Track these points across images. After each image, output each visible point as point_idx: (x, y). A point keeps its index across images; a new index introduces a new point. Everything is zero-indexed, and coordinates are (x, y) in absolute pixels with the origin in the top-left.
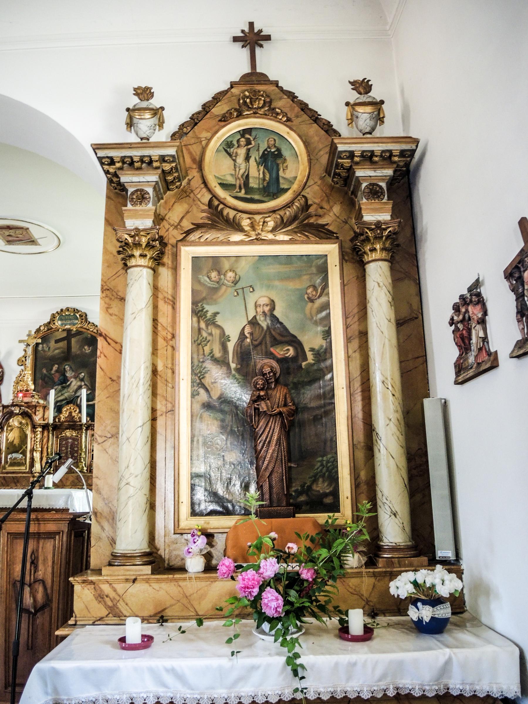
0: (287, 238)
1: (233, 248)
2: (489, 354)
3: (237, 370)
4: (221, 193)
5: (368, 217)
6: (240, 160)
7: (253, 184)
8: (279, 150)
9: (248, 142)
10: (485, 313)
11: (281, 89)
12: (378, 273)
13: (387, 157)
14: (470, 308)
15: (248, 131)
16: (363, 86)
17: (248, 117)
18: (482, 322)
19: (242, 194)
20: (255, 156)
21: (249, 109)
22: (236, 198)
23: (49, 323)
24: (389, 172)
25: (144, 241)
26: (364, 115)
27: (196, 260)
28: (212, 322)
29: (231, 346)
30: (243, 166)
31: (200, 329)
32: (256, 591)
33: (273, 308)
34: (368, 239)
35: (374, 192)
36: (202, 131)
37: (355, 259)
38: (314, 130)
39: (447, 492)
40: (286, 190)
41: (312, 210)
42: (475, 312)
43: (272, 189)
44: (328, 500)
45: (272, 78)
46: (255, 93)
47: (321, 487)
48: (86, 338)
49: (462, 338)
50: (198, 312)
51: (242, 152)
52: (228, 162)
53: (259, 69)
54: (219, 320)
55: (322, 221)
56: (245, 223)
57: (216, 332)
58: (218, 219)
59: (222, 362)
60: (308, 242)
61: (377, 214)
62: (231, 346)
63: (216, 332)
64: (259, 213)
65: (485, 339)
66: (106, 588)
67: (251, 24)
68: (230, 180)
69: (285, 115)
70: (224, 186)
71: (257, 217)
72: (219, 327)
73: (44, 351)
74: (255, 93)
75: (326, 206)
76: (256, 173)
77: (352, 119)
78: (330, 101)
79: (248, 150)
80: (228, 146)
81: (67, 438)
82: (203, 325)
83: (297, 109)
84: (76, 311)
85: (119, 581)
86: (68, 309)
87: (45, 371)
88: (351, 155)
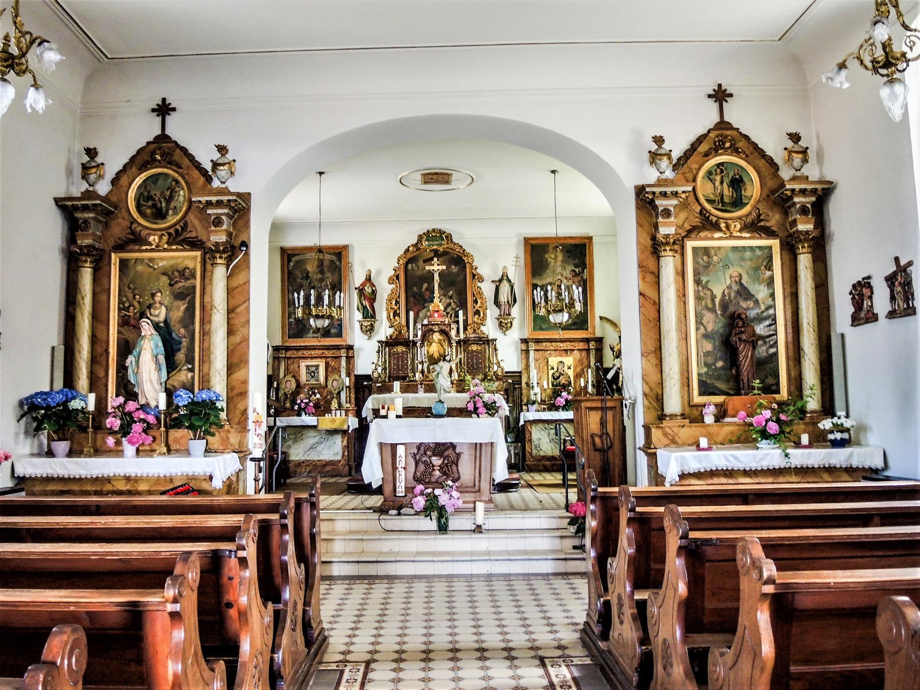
0: (748, 235)
1: (716, 241)
2: (873, 314)
3: (722, 315)
4: (707, 206)
5: (801, 227)
6: (717, 184)
7: (726, 200)
8: (741, 177)
9: (722, 171)
10: (872, 293)
11: (740, 133)
12: (805, 261)
13: (814, 192)
14: (864, 290)
15: (722, 164)
16: (795, 138)
17: (720, 155)
18: (871, 298)
19: (720, 206)
20: (726, 181)
21: (722, 149)
22: (716, 209)
23: (417, 244)
24: (813, 199)
25: (672, 241)
26: (797, 159)
27: (695, 249)
28: (705, 287)
29: (717, 301)
30: (719, 188)
31: (699, 291)
32: (764, 423)
33: (741, 279)
34: (801, 240)
35: (804, 211)
36: (693, 163)
37: (790, 248)
38: (762, 163)
39: (843, 382)
40: (747, 204)
41: (762, 217)
42: (866, 291)
43: (738, 203)
44: (774, 388)
45: (735, 126)
46: (724, 137)
47: (770, 380)
48: (453, 257)
49: (857, 302)
50: (698, 282)
51: (718, 178)
52: (710, 185)
53: (726, 119)
54: (710, 286)
55: (768, 224)
56: (723, 225)
57: (708, 293)
58: (708, 224)
59: (712, 310)
60: (761, 238)
61: (805, 226)
62: (717, 301)
63: (708, 293)
64: (730, 219)
65: (872, 306)
66: (668, 430)
67: (720, 85)
68: (712, 197)
69: (744, 153)
70: (709, 201)
71: (729, 222)
72: (709, 289)
73: (412, 269)
74: (724, 137)
75: (770, 214)
76: (727, 192)
77: (790, 159)
78: (773, 144)
79: (722, 177)
80: (709, 173)
81: (473, 351)
82: (700, 289)
83: (751, 148)
84: (441, 232)
85: (674, 427)
86: (434, 230)
87: (415, 289)
88: (793, 190)
